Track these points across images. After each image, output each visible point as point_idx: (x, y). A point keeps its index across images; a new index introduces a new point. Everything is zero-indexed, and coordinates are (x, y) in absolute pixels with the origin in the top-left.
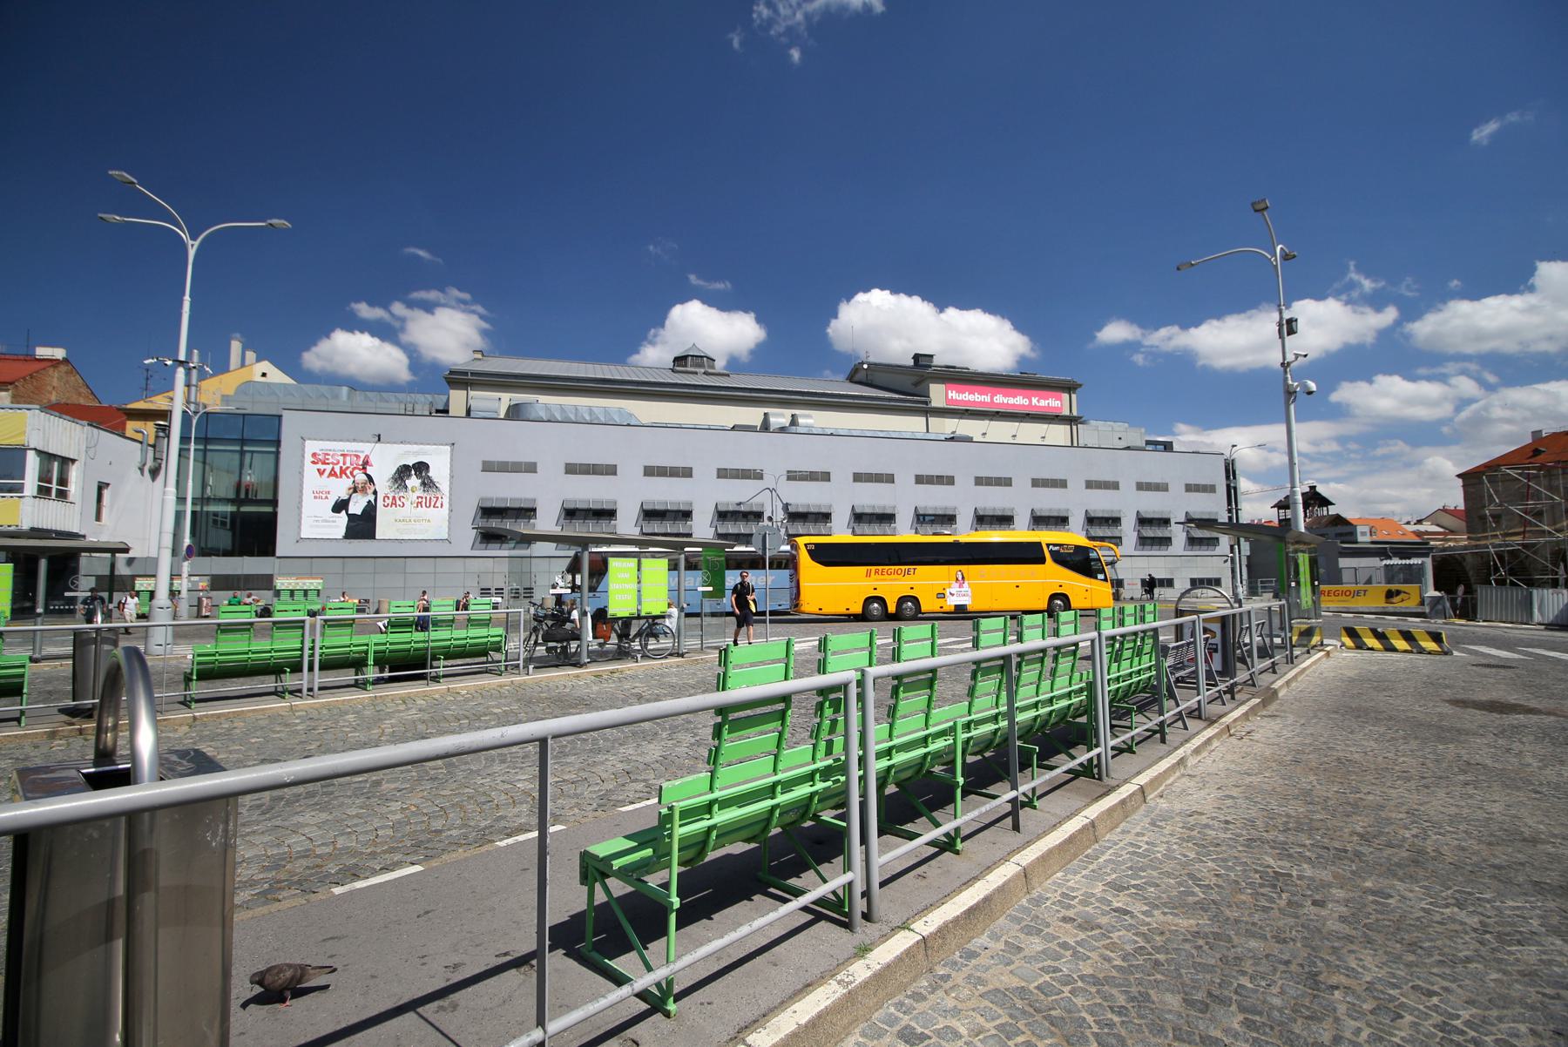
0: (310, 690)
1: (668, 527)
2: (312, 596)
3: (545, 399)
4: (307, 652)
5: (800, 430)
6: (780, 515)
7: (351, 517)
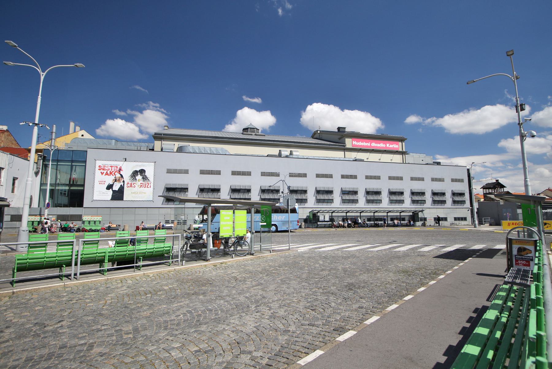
0: (75, 274)
1: (241, 196)
2: (97, 223)
3: (192, 144)
4: (74, 257)
5: (294, 157)
6: (286, 191)
7: (114, 191)
